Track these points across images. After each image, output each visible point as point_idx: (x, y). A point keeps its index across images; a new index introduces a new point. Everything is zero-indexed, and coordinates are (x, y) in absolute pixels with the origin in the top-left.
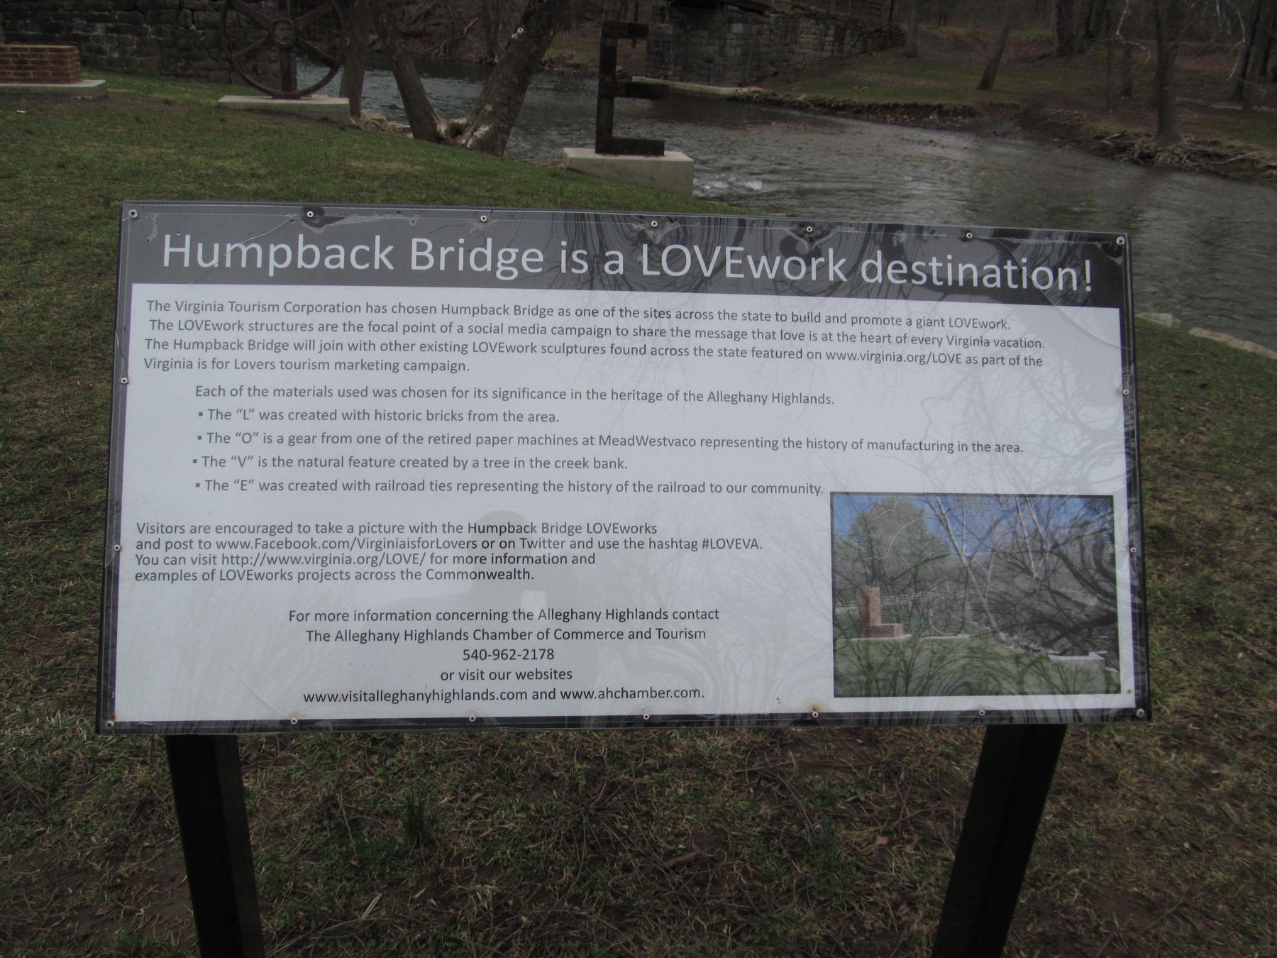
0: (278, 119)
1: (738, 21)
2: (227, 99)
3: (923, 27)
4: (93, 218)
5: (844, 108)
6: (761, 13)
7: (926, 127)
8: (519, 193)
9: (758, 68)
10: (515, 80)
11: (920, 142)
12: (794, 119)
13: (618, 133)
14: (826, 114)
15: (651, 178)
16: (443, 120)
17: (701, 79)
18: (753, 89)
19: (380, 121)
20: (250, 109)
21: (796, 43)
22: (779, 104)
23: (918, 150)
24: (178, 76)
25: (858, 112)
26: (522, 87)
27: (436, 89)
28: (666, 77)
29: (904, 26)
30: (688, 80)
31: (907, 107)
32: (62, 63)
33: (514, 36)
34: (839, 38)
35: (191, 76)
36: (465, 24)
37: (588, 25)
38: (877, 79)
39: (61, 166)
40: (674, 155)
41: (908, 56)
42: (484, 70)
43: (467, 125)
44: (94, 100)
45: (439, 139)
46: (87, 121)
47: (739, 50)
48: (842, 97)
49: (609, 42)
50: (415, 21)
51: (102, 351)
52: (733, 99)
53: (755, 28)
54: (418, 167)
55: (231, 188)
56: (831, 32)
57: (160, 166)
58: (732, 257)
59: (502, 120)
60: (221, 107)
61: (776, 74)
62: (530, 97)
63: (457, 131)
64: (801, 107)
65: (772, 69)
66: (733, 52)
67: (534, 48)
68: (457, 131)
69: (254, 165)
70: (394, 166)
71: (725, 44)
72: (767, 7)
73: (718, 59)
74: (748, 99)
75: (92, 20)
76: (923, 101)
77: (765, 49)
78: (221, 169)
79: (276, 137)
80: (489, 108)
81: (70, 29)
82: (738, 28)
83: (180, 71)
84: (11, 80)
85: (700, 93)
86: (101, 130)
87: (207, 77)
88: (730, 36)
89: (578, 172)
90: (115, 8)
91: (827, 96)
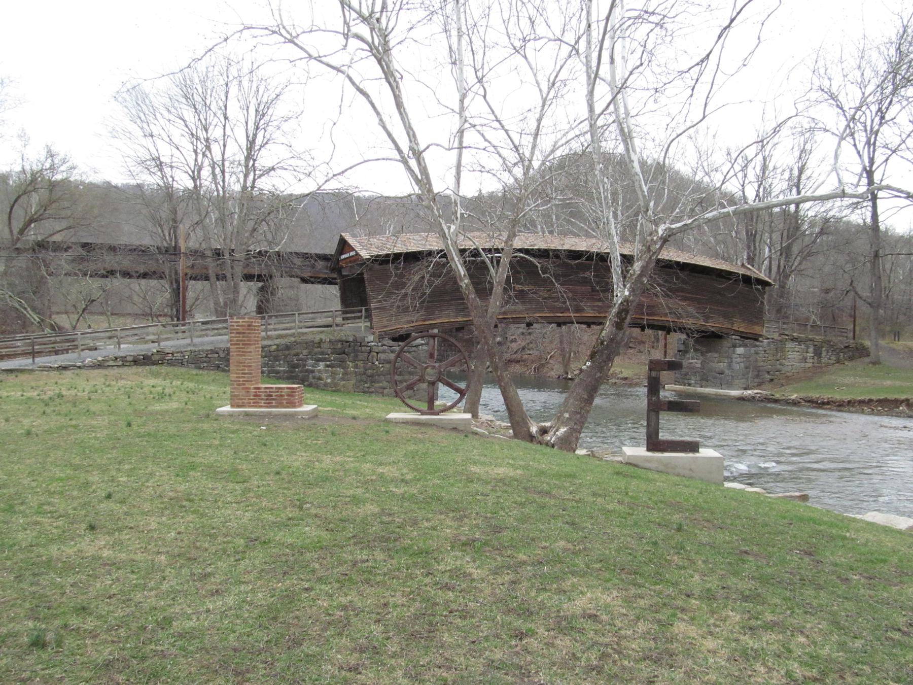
0: (423, 430)
1: (740, 346)
2: (392, 416)
3: (882, 342)
4: (290, 519)
5: (828, 403)
6: (757, 340)
7: (898, 415)
8: (594, 494)
9: (758, 376)
10: (585, 396)
11: (896, 428)
12: (790, 413)
13: (663, 436)
14: (814, 407)
15: (691, 470)
16: (534, 423)
17: (714, 386)
18: (756, 391)
19: (491, 421)
20: (406, 422)
22: (776, 401)
23: (891, 434)
24: (364, 392)
25: (839, 406)
26: (590, 400)
27: (529, 398)
28: (689, 385)
29: (867, 343)
30: (706, 386)
31: (880, 401)
32: (292, 396)
33: (584, 367)
34: (818, 353)
35: (372, 392)
36: (549, 353)
37: (631, 351)
38: (850, 381)
39: (278, 473)
40: (705, 452)
41: (874, 363)
42: (563, 383)
43: (551, 427)
44: (309, 419)
45: (531, 438)
46: (302, 434)
47: (742, 365)
48: (826, 395)
49: (654, 374)
50: (516, 352)
51: (272, 655)
52: (742, 399)
53: (753, 350)
54: (519, 472)
55: (386, 492)
56: (811, 350)
57: (341, 473)
59: (576, 424)
60: (388, 422)
61: (772, 380)
62: (597, 401)
63: (544, 431)
64: (795, 403)
65: (768, 377)
66: (738, 366)
67: (598, 375)
68: (544, 431)
69: (405, 471)
70: (501, 471)
72: (761, 336)
73: (727, 372)
74: (752, 399)
76: (891, 397)
77: (762, 364)
78: (381, 476)
79: (421, 446)
80: (567, 415)
81: (305, 366)
82: (740, 350)
84: (261, 407)
86: (309, 442)
87: (382, 393)
88: (735, 356)
89: (635, 466)
90: (332, 353)
91: (814, 395)
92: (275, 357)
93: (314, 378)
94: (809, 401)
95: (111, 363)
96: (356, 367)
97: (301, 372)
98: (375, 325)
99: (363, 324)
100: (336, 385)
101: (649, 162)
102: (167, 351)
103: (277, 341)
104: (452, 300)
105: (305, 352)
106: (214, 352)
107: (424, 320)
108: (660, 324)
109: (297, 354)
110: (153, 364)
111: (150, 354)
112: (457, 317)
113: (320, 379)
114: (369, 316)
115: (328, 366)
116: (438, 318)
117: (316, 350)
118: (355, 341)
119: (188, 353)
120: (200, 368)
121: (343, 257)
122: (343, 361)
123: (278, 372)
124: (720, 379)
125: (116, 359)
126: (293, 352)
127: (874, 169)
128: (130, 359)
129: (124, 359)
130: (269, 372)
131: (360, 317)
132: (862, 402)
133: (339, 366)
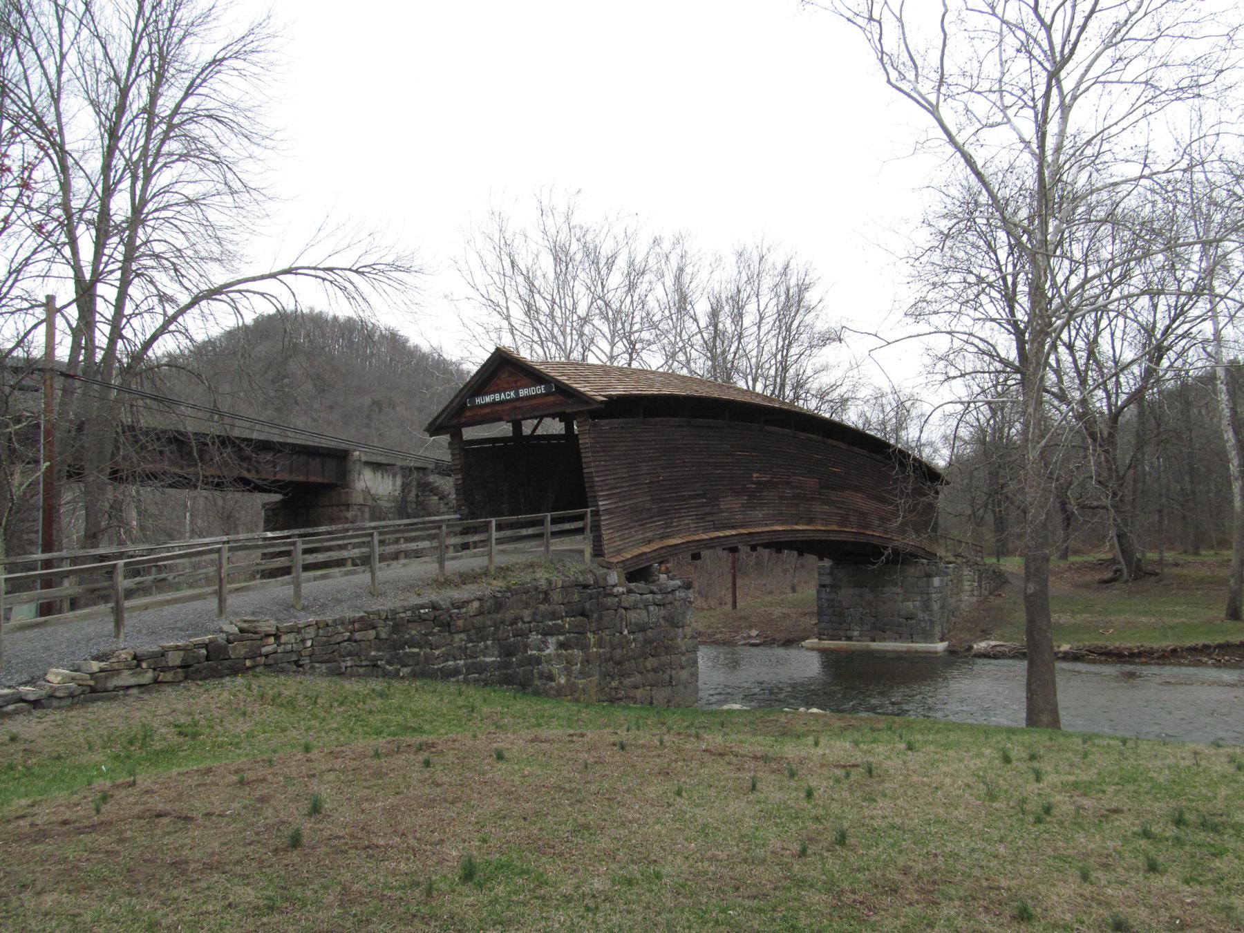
5: (1140, 655)
17: (900, 637)
28: (849, 638)
30: (884, 639)
71: (929, 599)
73: (921, 615)
75: (547, 633)
81: (526, 647)
93: (541, 676)
94: (1101, 654)
95: (126, 678)
97: (521, 664)
98: (607, 547)
99: (583, 544)
101: (187, 352)
104: (691, 497)
105: (527, 614)
106: (366, 623)
107: (662, 538)
111: (221, 638)
112: (696, 531)
113: (551, 678)
114: (596, 528)
115: (561, 645)
116: (678, 532)
117: (542, 607)
119: (311, 632)
121: (479, 401)
123: (481, 668)
124: (907, 627)
126: (509, 615)
128: (175, 659)
129: (158, 660)
132: (1194, 650)
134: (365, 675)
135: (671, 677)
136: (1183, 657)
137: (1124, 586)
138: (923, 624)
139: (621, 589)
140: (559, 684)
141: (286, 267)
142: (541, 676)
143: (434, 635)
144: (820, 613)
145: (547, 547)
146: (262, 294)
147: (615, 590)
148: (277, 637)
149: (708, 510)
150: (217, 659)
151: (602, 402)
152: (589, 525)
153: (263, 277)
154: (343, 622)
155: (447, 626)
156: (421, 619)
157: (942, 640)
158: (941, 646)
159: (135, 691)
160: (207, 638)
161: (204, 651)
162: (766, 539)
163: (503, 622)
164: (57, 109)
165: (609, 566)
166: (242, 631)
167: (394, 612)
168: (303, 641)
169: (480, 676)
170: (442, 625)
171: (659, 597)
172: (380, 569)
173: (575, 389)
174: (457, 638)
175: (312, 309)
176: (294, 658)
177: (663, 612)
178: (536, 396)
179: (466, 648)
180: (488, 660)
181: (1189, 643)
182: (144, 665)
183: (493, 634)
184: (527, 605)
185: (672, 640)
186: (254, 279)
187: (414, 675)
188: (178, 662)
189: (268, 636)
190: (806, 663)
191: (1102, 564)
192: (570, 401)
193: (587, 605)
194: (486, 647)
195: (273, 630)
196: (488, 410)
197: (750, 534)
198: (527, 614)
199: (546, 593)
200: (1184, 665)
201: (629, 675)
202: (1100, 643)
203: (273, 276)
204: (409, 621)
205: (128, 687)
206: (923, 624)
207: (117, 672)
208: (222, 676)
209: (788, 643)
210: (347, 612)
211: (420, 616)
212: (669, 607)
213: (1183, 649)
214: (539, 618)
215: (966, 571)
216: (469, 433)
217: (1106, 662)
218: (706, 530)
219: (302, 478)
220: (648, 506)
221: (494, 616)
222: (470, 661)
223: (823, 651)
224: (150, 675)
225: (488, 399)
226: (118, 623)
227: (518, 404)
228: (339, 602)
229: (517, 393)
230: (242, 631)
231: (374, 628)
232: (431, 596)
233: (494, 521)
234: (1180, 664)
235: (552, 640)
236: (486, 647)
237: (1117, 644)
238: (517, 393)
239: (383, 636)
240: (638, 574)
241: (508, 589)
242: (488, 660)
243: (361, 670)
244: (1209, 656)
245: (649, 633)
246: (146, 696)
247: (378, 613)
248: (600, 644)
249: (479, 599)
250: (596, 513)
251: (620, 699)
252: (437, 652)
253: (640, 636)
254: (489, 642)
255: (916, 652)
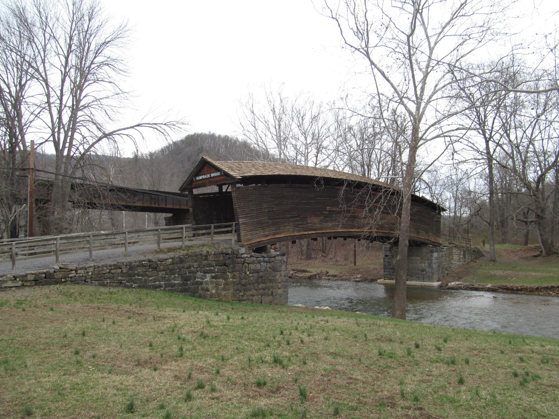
5: (521, 290)
17: (418, 279)
21: (452, 259)
30: (412, 280)
58: (150, 227)
71: (432, 262)
73: (428, 270)
75: (206, 272)
81: (195, 278)
83: (241, 297)
85: (421, 286)
92: (171, 270)
93: (202, 289)
94: (505, 289)
95: (10, 284)
96: (234, 277)
97: (193, 284)
98: (242, 238)
99: (233, 237)
100: (219, 295)
102: (71, 267)
103: (171, 254)
104: (291, 217)
105: (195, 264)
106: (117, 267)
107: (274, 235)
108: (355, 234)
109: (189, 267)
110: (56, 283)
111: (52, 271)
112: (294, 231)
113: (207, 290)
114: (237, 231)
115: (213, 277)
116: (283, 232)
118: (233, 253)
119: (92, 269)
120: (103, 285)
121: (197, 178)
122: (225, 273)
123: (173, 285)
124: (422, 275)
125: (15, 278)
126: (186, 265)
127: (82, 98)
128: (31, 278)
129: (24, 278)
130: (166, 286)
131: (230, 232)
132: (547, 288)
133: (221, 278)
134: (116, 286)
135: (272, 292)
136: (541, 292)
137: (542, 259)
138: (428, 274)
139: (246, 255)
140: (212, 293)
141: (137, 124)
142: (202, 289)
143: (149, 272)
144: (385, 268)
145: (212, 238)
146: (127, 135)
147: (243, 256)
148: (76, 271)
149: (300, 223)
150: (49, 278)
151: (239, 179)
152: (234, 229)
153: (128, 128)
154: (106, 266)
155: (155, 268)
156: (143, 266)
157: (438, 281)
158: (436, 284)
159: (14, 289)
160: (45, 271)
161: (44, 275)
162: (333, 235)
163: (183, 267)
164: (44, 66)
165: (242, 246)
166: (60, 268)
167: (130, 263)
168: (88, 272)
169: (171, 289)
170: (153, 268)
171: (267, 259)
172: (129, 246)
173: (229, 174)
174: (160, 273)
175: (210, 132)
176: (84, 279)
177: (269, 265)
178: (217, 176)
179: (165, 277)
180: (176, 282)
181: (545, 285)
182: (18, 279)
183: (179, 272)
184: (196, 261)
185: (273, 276)
186: (124, 129)
187: (139, 287)
188: (32, 279)
189: (72, 270)
190: (379, 291)
191: (536, 248)
192: (228, 178)
193: (227, 262)
194: (175, 277)
195: (74, 268)
196: (201, 182)
197: (323, 233)
198: (195, 264)
199: (206, 256)
200: (541, 295)
201: (250, 290)
202: (504, 284)
203: (132, 127)
204: (137, 266)
205: (11, 287)
206: (428, 274)
207: (6, 282)
208: (51, 284)
209: (373, 281)
210: (110, 262)
211: (142, 264)
212: (272, 263)
213: (542, 288)
214: (202, 266)
215: (455, 250)
216: (195, 192)
217: (506, 293)
218: (298, 231)
219: (178, 207)
220: (266, 221)
221: (179, 265)
222: (167, 282)
223: (385, 285)
224: (20, 283)
225: (201, 178)
226: (14, 264)
227: (211, 180)
228: (109, 258)
229: (210, 175)
230: (60, 268)
231: (120, 268)
232: (151, 257)
233: (213, 225)
234: (539, 295)
235: (208, 275)
236: (175, 277)
237: (512, 285)
238: (210, 175)
239: (125, 271)
240: (260, 249)
241: (187, 255)
242: (176, 282)
243: (114, 284)
244: (553, 291)
245: (261, 274)
246: (17, 291)
247: (123, 263)
248: (234, 277)
249: (173, 258)
250: (237, 225)
251: (245, 300)
252: (150, 279)
253: (256, 275)
254: (176, 275)
255: (425, 286)
